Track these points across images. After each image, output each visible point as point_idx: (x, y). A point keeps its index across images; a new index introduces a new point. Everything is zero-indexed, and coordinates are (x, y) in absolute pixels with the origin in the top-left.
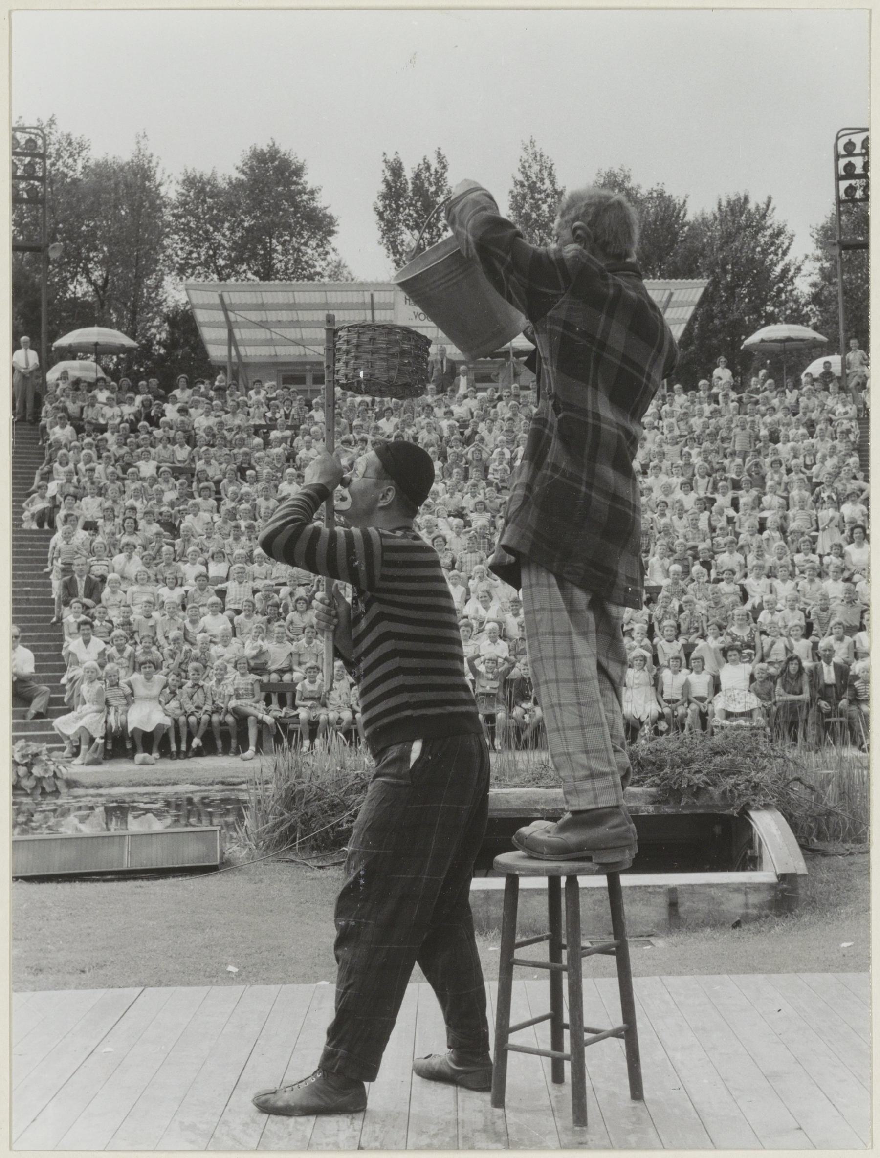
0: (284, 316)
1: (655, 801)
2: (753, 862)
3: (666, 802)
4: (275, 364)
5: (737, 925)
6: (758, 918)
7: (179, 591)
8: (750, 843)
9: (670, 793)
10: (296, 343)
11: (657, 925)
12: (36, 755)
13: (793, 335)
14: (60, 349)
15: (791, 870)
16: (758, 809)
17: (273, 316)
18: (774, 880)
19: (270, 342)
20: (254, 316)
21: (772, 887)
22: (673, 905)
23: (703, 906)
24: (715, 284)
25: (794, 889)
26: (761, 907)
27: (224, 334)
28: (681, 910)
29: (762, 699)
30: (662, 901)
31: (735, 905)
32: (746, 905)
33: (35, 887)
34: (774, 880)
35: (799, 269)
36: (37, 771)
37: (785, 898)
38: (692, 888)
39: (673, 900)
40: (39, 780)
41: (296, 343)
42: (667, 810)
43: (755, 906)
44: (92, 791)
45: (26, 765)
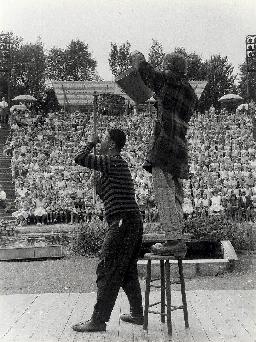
0: (81, 91)
1: (192, 237)
2: (221, 256)
3: (195, 238)
4: (78, 106)
5: (217, 275)
6: (223, 273)
7: (50, 174)
8: (221, 250)
9: (197, 235)
10: (85, 99)
11: (193, 275)
12: (7, 224)
13: (233, 97)
14: (14, 101)
15: (233, 258)
16: (223, 240)
17: (78, 91)
18: (228, 261)
19: (77, 99)
20: (72, 91)
21: (227, 263)
22: (198, 269)
23: (207, 269)
24: (210, 82)
25: (234, 264)
26: (224, 270)
27: (63, 96)
28: (200, 270)
29: (224, 207)
30: (194, 268)
31: (216, 269)
32: (220, 269)
33: (7, 263)
34: (228, 261)
35: (235, 78)
36: (7, 228)
37: (231, 267)
38: (203, 264)
39: (198, 267)
40: (8, 231)
41: (85, 99)
42: (196, 240)
43: (222, 269)
44: (24, 234)
45: (4, 226)
